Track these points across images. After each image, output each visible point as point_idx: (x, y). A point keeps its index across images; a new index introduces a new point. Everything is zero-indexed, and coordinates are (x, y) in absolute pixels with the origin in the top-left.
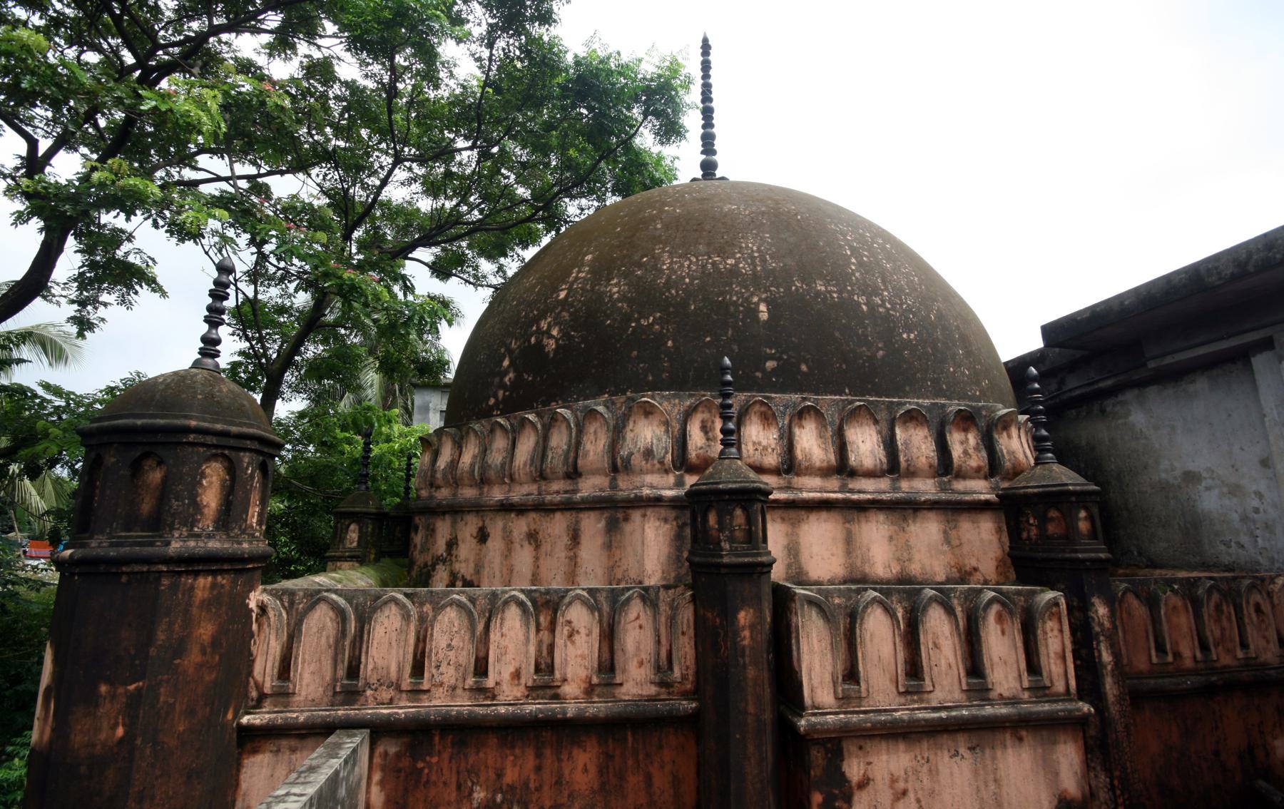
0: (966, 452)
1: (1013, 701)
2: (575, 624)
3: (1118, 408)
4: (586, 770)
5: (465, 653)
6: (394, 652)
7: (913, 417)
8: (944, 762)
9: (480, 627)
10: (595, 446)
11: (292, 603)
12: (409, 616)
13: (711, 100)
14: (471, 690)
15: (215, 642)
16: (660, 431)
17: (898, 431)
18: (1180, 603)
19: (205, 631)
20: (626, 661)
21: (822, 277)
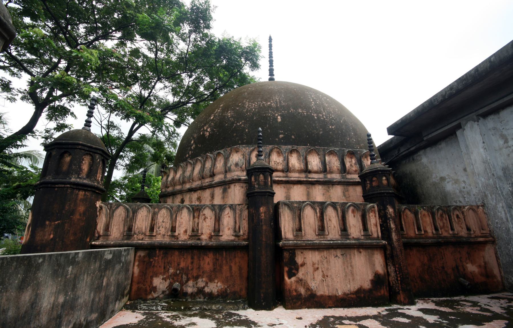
0: (351, 165)
1: (358, 239)
2: (206, 215)
3: (418, 158)
4: (209, 264)
5: (168, 224)
6: (144, 223)
7: (331, 153)
8: (332, 260)
9: (174, 216)
10: (220, 164)
11: (111, 207)
12: (150, 211)
13: (272, 57)
14: (170, 236)
15: (84, 213)
16: (241, 157)
17: (327, 158)
18: (426, 213)
19: (81, 208)
20: (224, 228)
21: (301, 108)
